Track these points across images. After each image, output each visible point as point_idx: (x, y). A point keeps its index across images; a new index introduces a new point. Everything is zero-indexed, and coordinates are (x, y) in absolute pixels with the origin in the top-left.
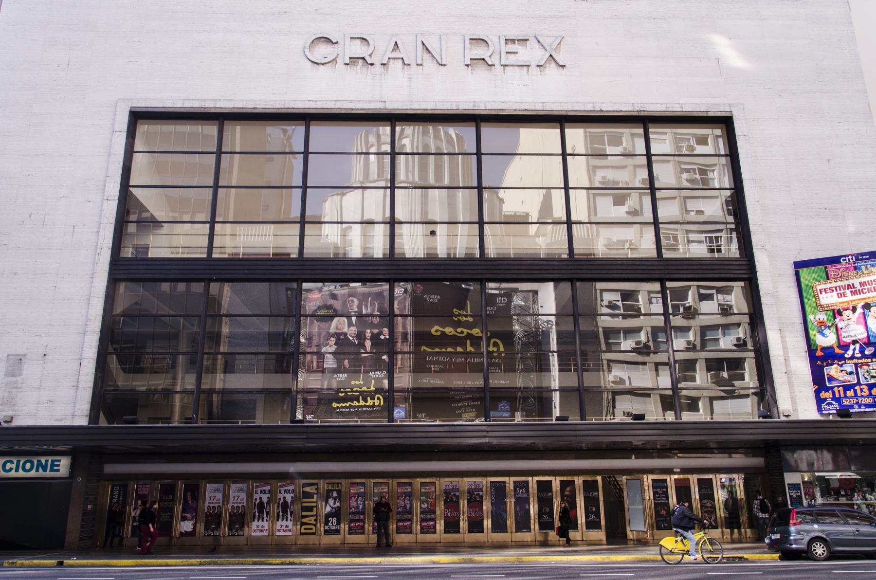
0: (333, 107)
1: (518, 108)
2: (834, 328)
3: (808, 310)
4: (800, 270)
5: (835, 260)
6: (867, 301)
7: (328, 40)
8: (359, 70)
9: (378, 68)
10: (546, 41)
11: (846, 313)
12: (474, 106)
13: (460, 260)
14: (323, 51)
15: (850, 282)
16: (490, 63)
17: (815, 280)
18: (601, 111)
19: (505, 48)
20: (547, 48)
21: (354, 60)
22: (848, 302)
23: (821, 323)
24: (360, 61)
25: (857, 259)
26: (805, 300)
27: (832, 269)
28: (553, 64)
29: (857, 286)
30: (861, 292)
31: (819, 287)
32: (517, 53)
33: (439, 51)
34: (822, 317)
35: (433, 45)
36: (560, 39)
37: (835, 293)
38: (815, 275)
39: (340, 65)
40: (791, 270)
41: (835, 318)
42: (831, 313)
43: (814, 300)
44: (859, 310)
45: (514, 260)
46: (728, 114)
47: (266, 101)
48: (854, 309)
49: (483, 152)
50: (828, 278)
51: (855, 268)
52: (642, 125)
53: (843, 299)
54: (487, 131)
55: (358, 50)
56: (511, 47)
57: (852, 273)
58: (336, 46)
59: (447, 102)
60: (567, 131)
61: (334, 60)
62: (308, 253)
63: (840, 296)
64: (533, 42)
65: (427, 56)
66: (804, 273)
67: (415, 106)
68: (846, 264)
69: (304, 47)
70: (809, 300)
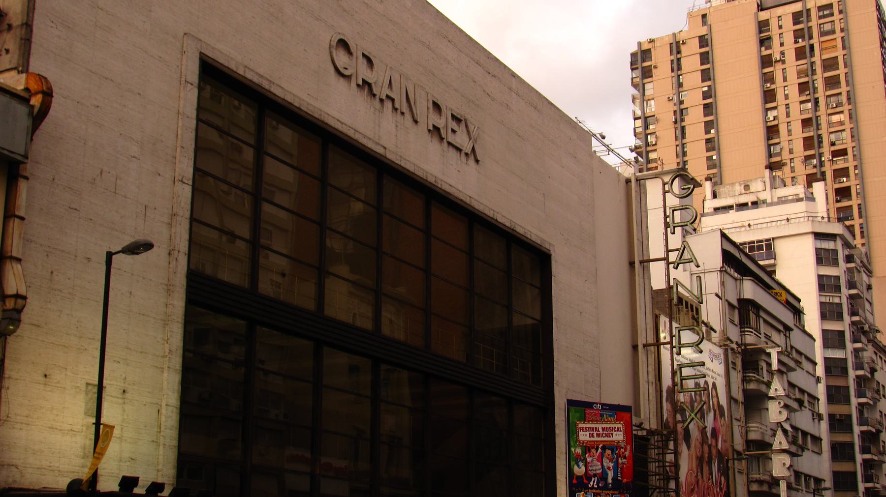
3: (572, 443)
5: (589, 405)
11: (593, 451)
23: (578, 455)
29: (600, 430)
31: (580, 425)
34: (579, 451)
38: (578, 415)
44: (600, 450)
63: (591, 435)
66: (572, 409)
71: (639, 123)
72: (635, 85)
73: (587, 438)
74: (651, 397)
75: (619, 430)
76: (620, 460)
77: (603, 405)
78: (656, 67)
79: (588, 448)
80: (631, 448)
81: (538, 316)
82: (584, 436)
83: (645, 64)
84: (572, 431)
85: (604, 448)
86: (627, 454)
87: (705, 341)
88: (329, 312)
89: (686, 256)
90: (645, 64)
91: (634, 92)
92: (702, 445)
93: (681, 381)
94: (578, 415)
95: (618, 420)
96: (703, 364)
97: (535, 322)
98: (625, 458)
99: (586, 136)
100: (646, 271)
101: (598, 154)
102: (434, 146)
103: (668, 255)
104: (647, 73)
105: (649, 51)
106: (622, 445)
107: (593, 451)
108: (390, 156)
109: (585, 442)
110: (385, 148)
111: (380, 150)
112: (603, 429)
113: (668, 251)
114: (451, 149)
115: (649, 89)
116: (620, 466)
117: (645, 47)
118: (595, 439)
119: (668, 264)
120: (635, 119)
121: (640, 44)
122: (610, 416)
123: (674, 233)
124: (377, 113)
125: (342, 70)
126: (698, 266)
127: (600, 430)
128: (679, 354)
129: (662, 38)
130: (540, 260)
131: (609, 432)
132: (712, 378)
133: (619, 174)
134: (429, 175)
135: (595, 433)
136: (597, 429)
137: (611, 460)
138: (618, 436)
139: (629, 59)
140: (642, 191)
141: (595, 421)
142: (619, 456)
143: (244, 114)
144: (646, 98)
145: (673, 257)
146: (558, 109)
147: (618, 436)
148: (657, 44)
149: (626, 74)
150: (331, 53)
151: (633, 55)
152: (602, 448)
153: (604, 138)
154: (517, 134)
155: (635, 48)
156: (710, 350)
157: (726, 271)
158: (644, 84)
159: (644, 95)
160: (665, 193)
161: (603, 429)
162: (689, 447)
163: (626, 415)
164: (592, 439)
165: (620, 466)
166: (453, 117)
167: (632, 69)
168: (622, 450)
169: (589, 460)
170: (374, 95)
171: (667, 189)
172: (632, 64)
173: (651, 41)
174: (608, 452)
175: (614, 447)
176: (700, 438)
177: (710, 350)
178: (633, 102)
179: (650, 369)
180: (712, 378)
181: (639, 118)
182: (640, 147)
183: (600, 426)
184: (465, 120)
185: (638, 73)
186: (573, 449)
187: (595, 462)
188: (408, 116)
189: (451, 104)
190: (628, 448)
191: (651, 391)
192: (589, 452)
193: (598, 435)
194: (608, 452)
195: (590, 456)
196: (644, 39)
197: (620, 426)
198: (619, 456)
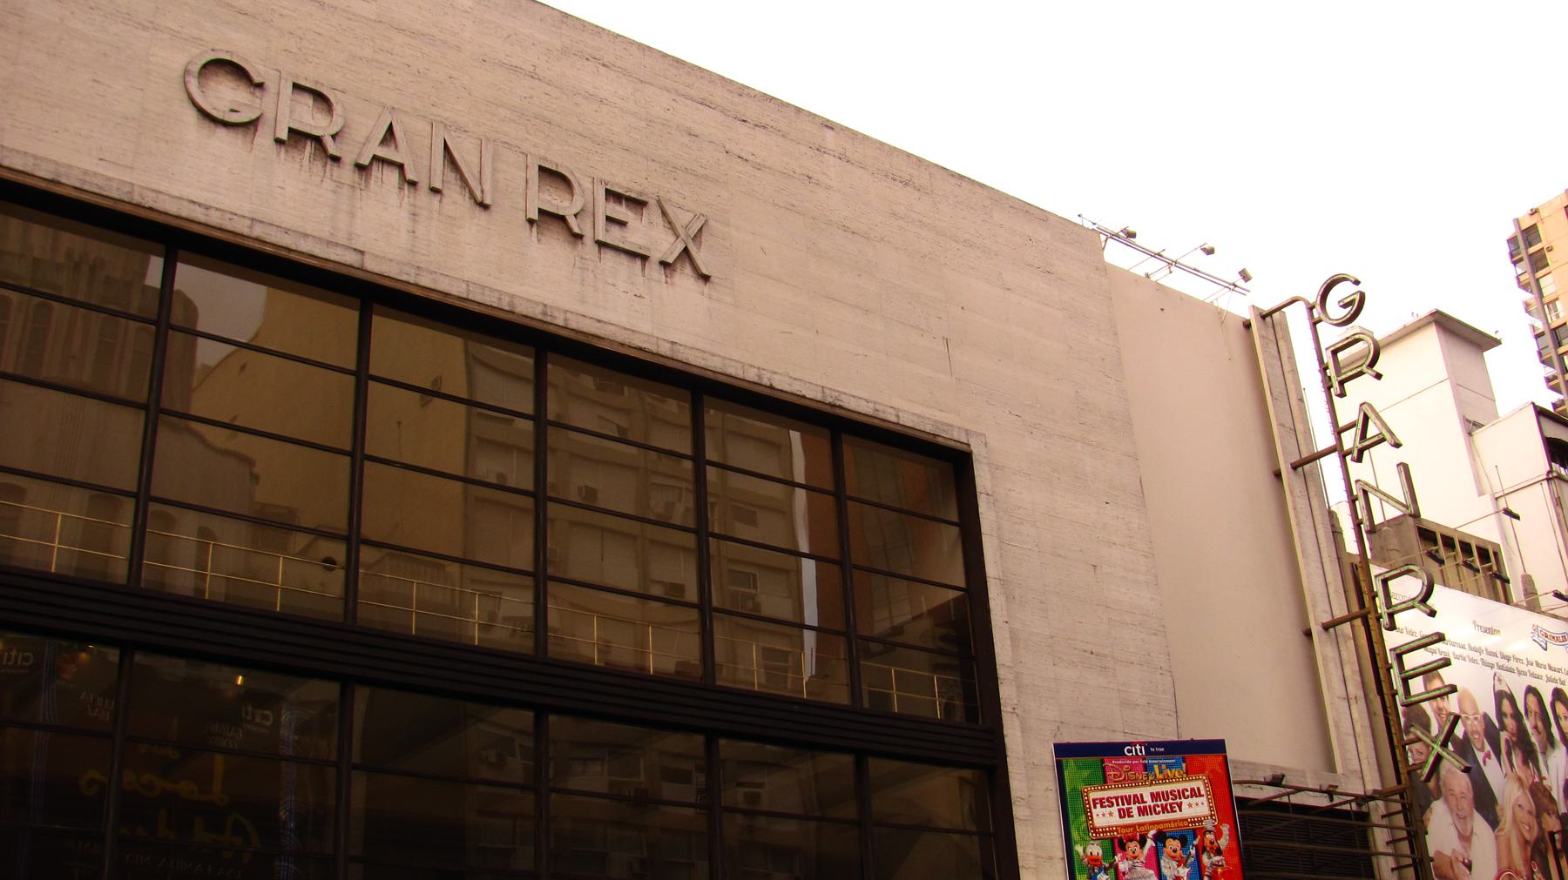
0: (246, 231)
1: (627, 342)
2: (1112, 871)
3: (1075, 835)
4: (1064, 760)
5: (1115, 749)
6: (1161, 827)
7: (237, 71)
8: (306, 162)
9: (347, 173)
10: (681, 218)
11: (1133, 846)
12: (544, 314)
13: (659, 679)
14: (224, 96)
15: (1137, 791)
16: (576, 230)
17: (1088, 782)
18: (771, 387)
19: (606, 208)
20: (681, 231)
21: (297, 137)
22: (1133, 826)
23: (1094, 861)
24: (309, 147)
25: (1148, 752)
26: (1071, 817)
27: (1112, 763)
28: (688, 269)
29: (1147, 798)
30: (1152, 810)
31: (1092, 795)
32: (1517, 517)
33: (476, 171)
34: (1096, 850)
35: (465, 154)
36: (702, 220)
37: (1115, 809)
38: (1086, 773)
39: (264, 138)
40: (1049, 757)
41: (1114, 854)
42: (1107, 844)
43: (1083, 818)
44: (1150, 843)
45: (281, 618)
46: (964, 448)
47: (86, 172)
48: (1142, 843)
49: (373, 371)
50: (1105, 782)
51: (1146, 768)
52: (358, 302)
53: (1127, 821)
54: (385, 328)
55: (310, 119)
56: (621, 212)
57: (1142, 775)
58: (258, 92)
59: (491, 290)
60: (376, 319)
61: (251, 126)
62: (369, 613)
63: (1124, 813)
64: (653, 213)
65: (451, 176)
66: (1070, 763)
67: (425, 281)
68: (1131, 758)
69: (186, 72)
70: (1077, 816)
71: (1548, 340)
72: (1524, 286)
73: (1115, 820)
74: (1358, 729)
75: (1195, 793)
76: (1205, 859)
77: (1148, 746)
78: (1550, 249)
79: (1117, 842)
80: (1233, 830)
81: (960, 581)
82: (1105, 818)
83: (1532, 250)
84: (1070, 808)
85: (1161, 837)
86: (1223, 842)
87: (1437, 588)
88: (553, 650)
89: (1372, 431)
90: (1532, 250)
91: (1527, 296)
92: (1538, 817)
93: (1405, 681)
94: (1086, 773)
95: (1190, 773)
96: (1440, 638)
97: (959, 593)
98: (1218, 852)
99: (1083, 240)
100: (1313, 486)
101: (1153, 278)
102: (550, 252)
103: (1339, 439)
104: (1539, 262)
105: (1534, 227)
106: (1208, 824)
107: (1133, 846)
108: (372, 265)
109: (1111, 829)
110: (362, 253)
111: (350, 258)
112: (1154, 797)
113: (1338, 432)
114: (609, 255)
115: (1549, 285)
116: (1208, 871)
117: (1525, 225)
118: (1137, 819)
119: (1343, 457)
120: (1537, 337)
121: (1517, 221)
122: (1169, 766)
123: (1342, 395)
124: (346, 191)
125: (234, 118)
126: (1397, 445)
127: (1147, 798)
128: (1392, 627)
129: (1550, 202)
130: (949, 467)
131: (1170, 801)
132: (1549, 680)
133: (1220, 316)
134: (517, 302)
135: (1134, 808)
136: (1138, 799)
137: (1181, 862)
138: (1198, 808)
139: (1505, 249)
140: (1279, 336)
141: (1135, 783)
142: (1201, 849)
143: (675, 408)
144: (1546, 300)
145: (1349, 440)
146: (982, 186)
147: (1198, 808)
148: (1544, 213)
149: (1509, 272)
150: (185, 83)
151: (1512, 241)
152: (1155, 838)
153: (1132, 235)
154: (846, 229)
155: (1511, 231)
156: (1536, 629)
157: (1559, 477)
158: (1537, 280)
159: (1541, 296)
160: (1314, 324)
161: (1154, 797)
162: (1494, 822)
163: (1212, 760)
164: (1127, 821)
165: (1208, 871)
166: (612, 195)
167: (1515, 263)
168: (1210, 836)
169: (1123, 866)
170: (578, 237)
171: (1316, 316)
172: (1512, 256)
173: (1534, 212)
174: (1173, 844)
175: (1188, 834)
176: (1527, 802)
177: (1536, 629)
178: (1528, 311)
179: (1348, 672)
180: (1549, 680)
181: (1542, 334)
182: (1555, 377)
183: (1146, 792)
184: (659, 202)
185: (1525, 265)
186: (1079, 849)
187: (1140, 869)
188: (454, 193)
189: (594, 170)
190: (1225, 829)
191: (1355, 716)
192: (1123, 848)
193: (1142, 811)
194: (1173, 844)
195: (1125, 858)
196: (1522, 212)
197: (1198, 784)
198: (1201, 849)
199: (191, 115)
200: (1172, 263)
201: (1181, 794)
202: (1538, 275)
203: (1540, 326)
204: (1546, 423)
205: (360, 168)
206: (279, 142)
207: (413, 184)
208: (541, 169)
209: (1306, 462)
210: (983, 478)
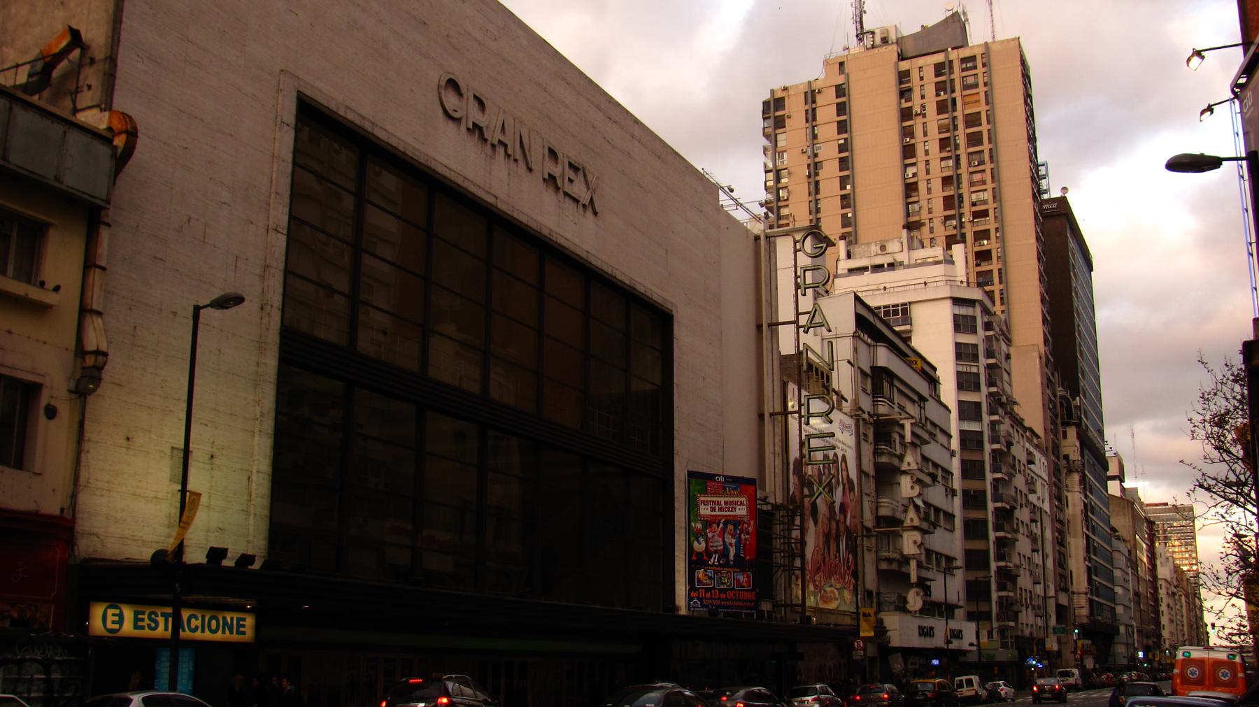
5: (711, 477)
11: (715, 526)
17: (700, 492)
34: (699, 526)
63: (713, 509)
66: (693, 481)
72: (767, 136)
73: (709, 512)
75: (742, 504)
78: (789, 117)
82: (705, 510)
83: (778, 114)
84: (692, 505)
85: (726, 523)
86: (751, 529)
89: (818, 319)
90: (778, 114)
91: (767, 143)
95: (741, 493)
96: (833, 435)
102: (549, 197)
104: (780, 123)
105: (782, 99)
107: (715, 526)
108: (501, 206)
111: (491, 200)
112: (726, 503)
113: (798, 314)
115: (782, 140)
117: (779, 95)
118: (717, 513)
119: (798, 327)
120: (767, 172)
121: (772, 92)
128: (807, 423)
131: (731, 505)
133: (747, 231)
136: (719, 503)
137: (733, 536)
138: (742, 511)
141: (715, 494)
145: (803, 320)
147: (742, 511)
148: (791, 92)
153: (732, 191)
154: (639, 185)
155: (767, 96)
160: (796, 251)
161: (726, 503)
162: (816, 523)
163: (750, 488)
166: (571, 165)
167: (764, 119)
169: (710, 535)
170: (486, 140)
173: (785, 89)
174: (731, 527)
175: (736, 522)
176: (827, 515)
182: (771, 202)
183: (722, 500)
185: (771, 122)
188: (522, 164)
189: (568, 150)
193: (720, 509)
194: (731, 527)
196: (777, 86)
197: (743, 499)
199: (440, 111)
200: (738, 204)
201: (736, 503)
202: (778, 131)
203: (770, 165)
204: (859, 305)
205: (493, 146)
206: (468, 129)
207: (509, 156)
208: (570, 164)
209: (774, 325)
210: (684, 338)
